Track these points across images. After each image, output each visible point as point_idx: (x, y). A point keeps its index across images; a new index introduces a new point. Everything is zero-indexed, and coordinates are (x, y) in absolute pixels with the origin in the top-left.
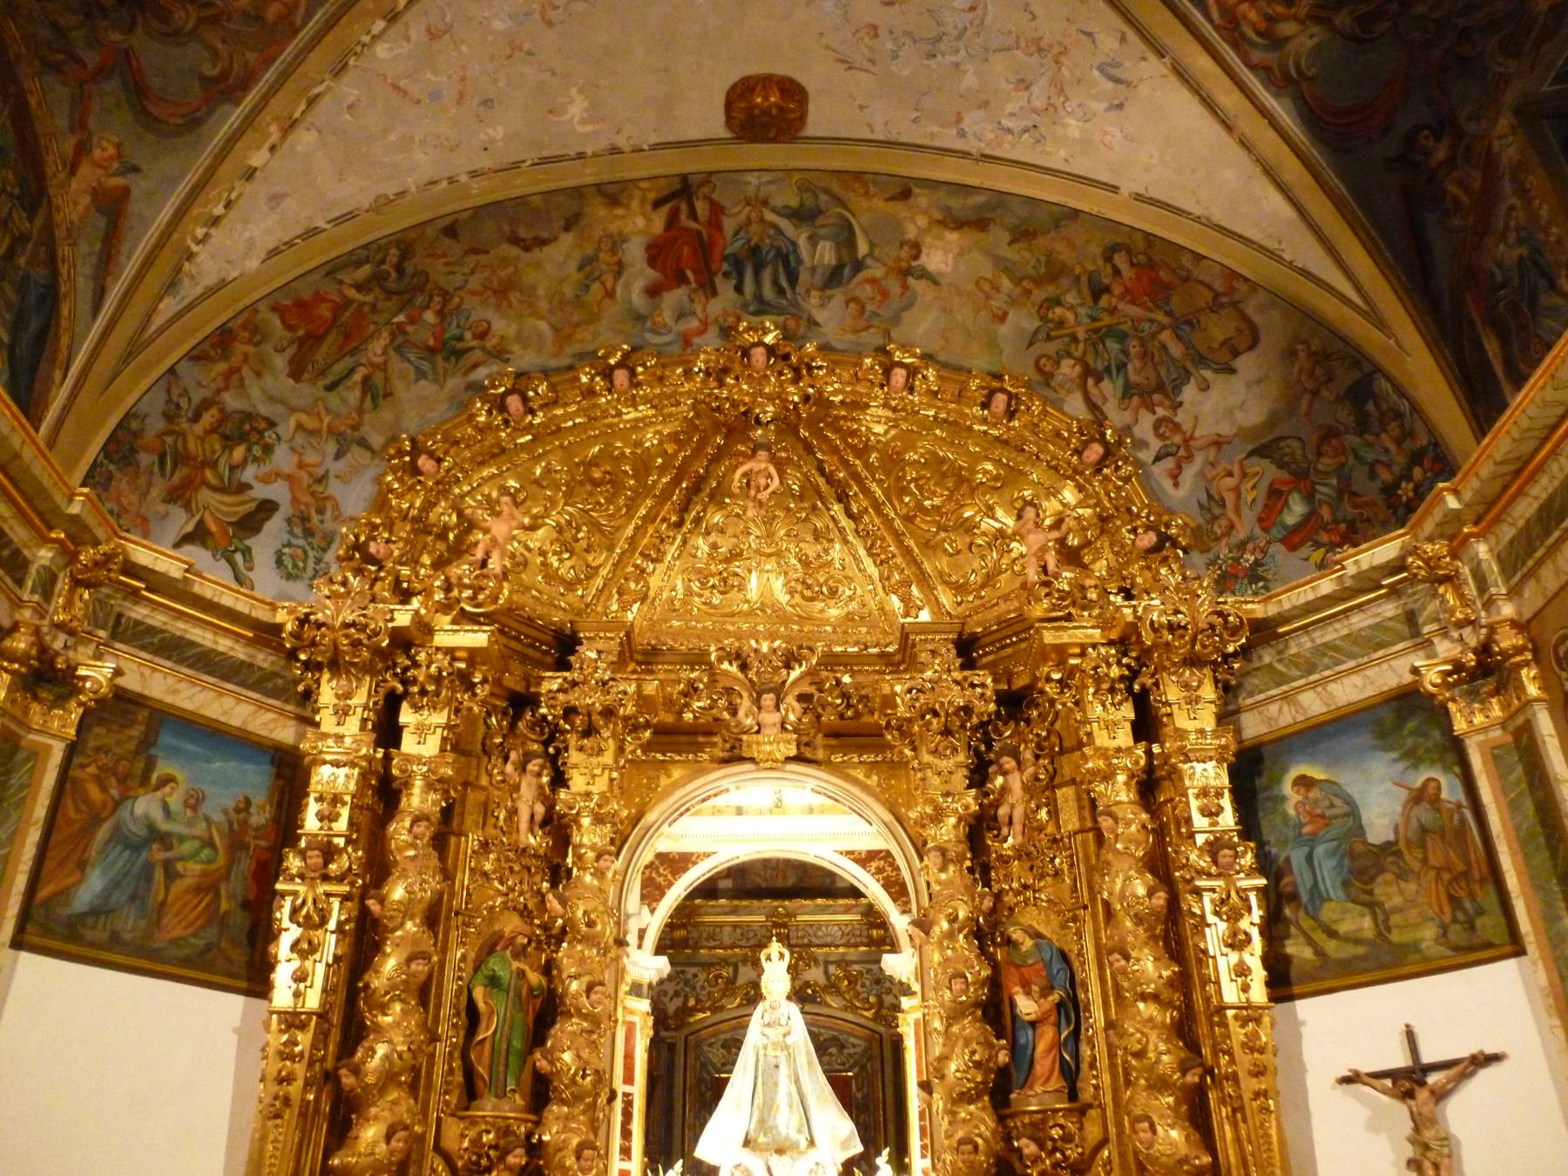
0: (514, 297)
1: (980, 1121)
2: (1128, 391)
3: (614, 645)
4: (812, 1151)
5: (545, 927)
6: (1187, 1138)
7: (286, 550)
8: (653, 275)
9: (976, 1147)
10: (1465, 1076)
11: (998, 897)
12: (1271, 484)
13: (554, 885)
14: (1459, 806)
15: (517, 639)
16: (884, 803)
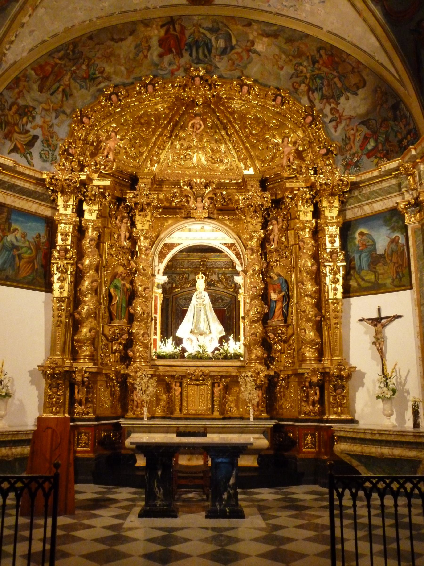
0: (113, 59)
1: (258, 328)
2: (323, 97)
3: (149, 180)
4: (210, 335)
5: (130, 270)
6: (315, 335)
7: (42, 152)
8: (161, 50)
9: (256, 335)
10: (391, 321)
11: (268, 263)
12: (365, 135)
13: (132, 258)
14: (403, 245)
15: (118, 178)
16: (235, 232)
